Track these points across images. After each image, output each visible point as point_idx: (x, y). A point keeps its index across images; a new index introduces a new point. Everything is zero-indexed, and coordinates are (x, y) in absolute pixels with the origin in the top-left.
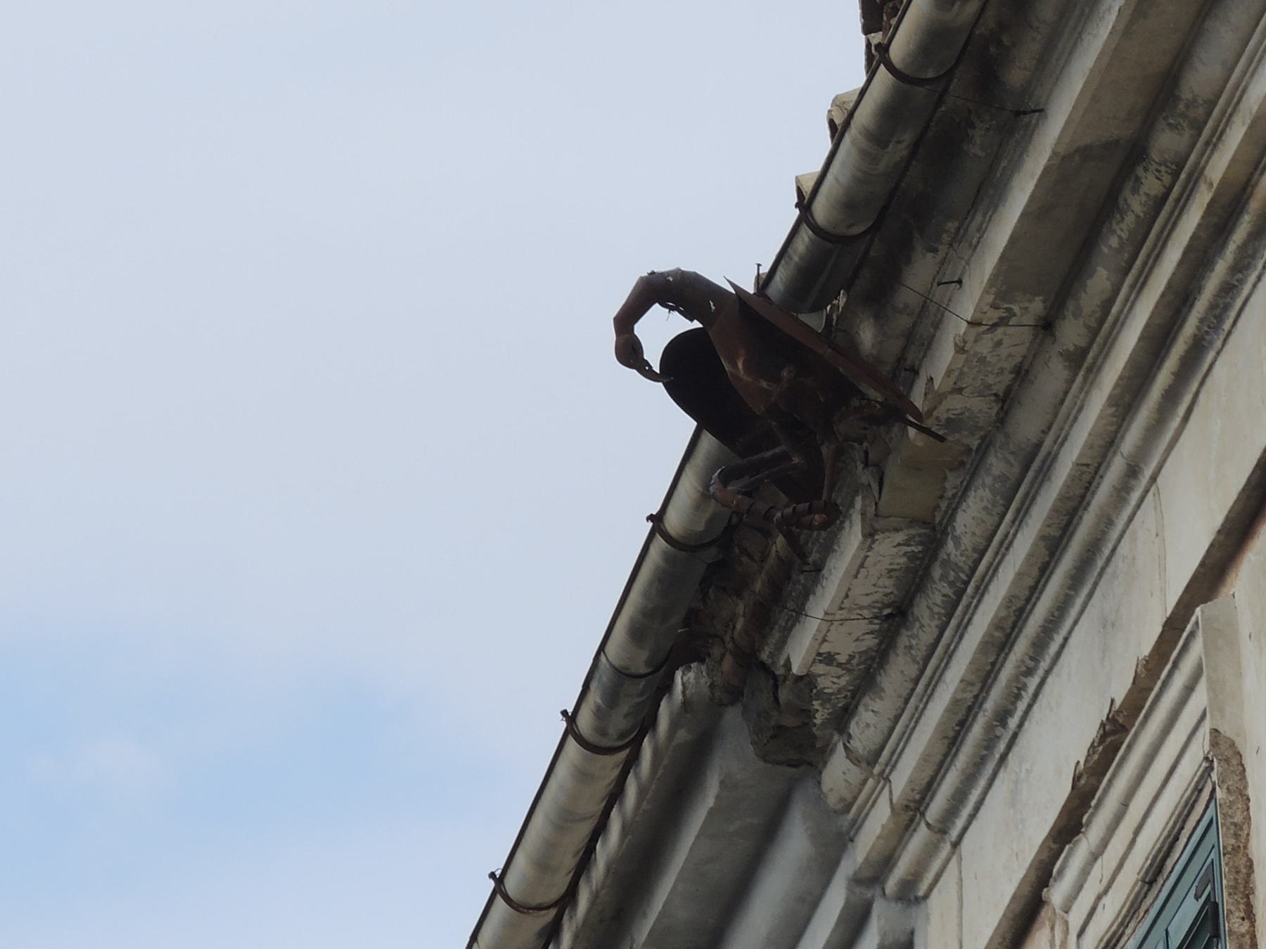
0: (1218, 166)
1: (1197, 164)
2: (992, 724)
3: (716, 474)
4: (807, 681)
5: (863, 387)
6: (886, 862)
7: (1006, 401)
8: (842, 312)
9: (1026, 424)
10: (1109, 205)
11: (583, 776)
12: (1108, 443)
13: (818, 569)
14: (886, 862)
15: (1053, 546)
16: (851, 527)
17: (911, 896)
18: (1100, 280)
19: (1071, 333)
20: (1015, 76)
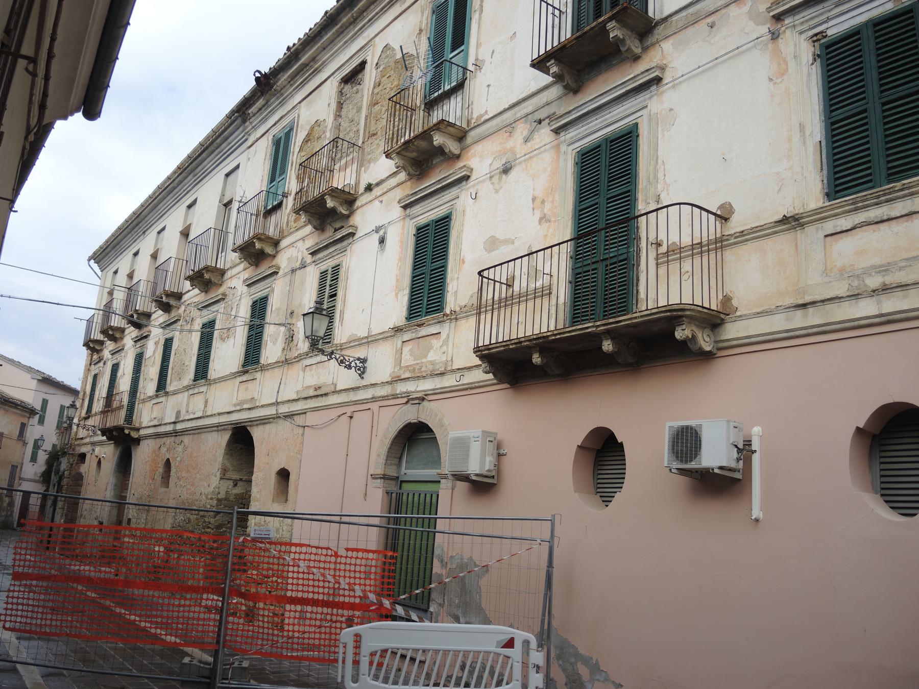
0: (316, 66)
1: (324, 62)
2: (225, 669)
3: (602, 18)
4: (249, 114)
5: (189, 650)
6: (248, 132)
7: (282, 89)
8: (165, 641)
9: (283, 91)
10: (302, 70)
11: (225, 120)
12: (291, 93)
13: (321, 37)
14: (248, 132)
15: (280, 103)
16: (109, 305)
17: (249, 135)
18: (298, 77)
19: (292, 82)
20: (300, 56)
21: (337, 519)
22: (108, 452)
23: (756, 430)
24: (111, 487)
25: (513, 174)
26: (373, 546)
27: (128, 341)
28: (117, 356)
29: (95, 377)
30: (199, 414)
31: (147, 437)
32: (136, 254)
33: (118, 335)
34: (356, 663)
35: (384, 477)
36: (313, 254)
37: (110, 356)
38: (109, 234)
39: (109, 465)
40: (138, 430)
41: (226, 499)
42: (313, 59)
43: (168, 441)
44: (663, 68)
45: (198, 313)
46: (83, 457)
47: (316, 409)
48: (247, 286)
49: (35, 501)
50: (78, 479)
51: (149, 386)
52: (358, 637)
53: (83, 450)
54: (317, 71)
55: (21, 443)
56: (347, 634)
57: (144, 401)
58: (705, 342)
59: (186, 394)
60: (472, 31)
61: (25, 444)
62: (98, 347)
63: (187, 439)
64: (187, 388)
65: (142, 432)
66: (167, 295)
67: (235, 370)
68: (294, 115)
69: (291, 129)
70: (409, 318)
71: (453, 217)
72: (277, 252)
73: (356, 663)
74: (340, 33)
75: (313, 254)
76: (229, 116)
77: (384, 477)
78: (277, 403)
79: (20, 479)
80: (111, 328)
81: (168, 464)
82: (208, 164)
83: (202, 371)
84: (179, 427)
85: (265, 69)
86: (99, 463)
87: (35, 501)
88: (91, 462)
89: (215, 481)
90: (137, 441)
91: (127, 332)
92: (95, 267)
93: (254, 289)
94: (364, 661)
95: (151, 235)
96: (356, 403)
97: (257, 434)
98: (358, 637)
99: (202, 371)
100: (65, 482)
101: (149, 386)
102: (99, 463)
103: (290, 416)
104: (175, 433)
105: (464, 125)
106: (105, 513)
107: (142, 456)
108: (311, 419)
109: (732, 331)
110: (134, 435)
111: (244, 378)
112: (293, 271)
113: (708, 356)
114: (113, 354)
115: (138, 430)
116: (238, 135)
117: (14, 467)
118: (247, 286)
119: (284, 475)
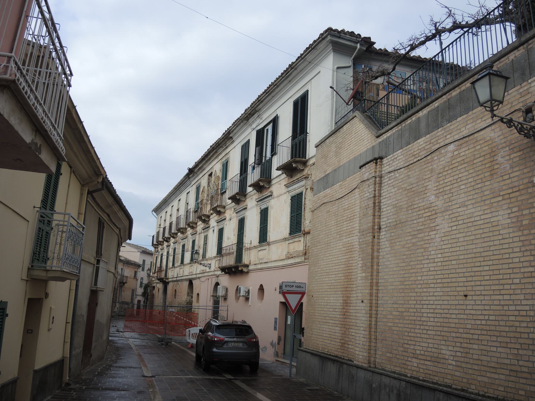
21: (205, 308)
22: (160, 286)
23: (251, 288)
24: (162, 299)
25: (232, 220)
26: (161, 305)
27: (213, 222)
28: (162, 251)
29: (157, 257)
30: (181, 275)
31: (171, 281)
32: (179, 200)
33: (194, 226)
34: (189, 336)
35: (213, 296)
36: (203, 230)
37: (216, 224)
38: (162, 199)
39: (161, 291)
40: (168, 279)
41: (189, 302)
42: (202, 166)
43: (176, 283)
44: (247, 205)
45: (181, 241)
46: (154, 287)
47: (203, 277)
48: (236, 213)
49: (142, 303)
50: (153, 295)
51: (170, 264)
52: (189, 331)
53: (154, 285)
54: (204, 170)
55: (135, 280)
56: (187, 330)
57: (250, 249)
58: (245, 270)
59: (179, 268)
60: (99, 278)
61: (137, 280)
62: (157, 247)
63: (180, 283)
64: (179, 266)
65: (170, 280)
66: (173, 234)
67: (189, 262)
68: (228, 156)
69: (227, 163)
70: (290, 234)
71: (269, 209)
72: (225, 210)
73: (189, 336)
74: (207, 162)
75: (203, 230)
76: (185, 176)
77: (213, 296)
78: (196, 274)
79: (136, 295)
80: (159, 241)
81: (176, 290)
82: (182, 188)
83: (182, 262)
84: (178, 279)
85: (191, 167)
86: (159, 290)
87: (142, 303)
88: (156, 289)
89: (186, 296)
90: (168, 283)
91: (198, 224)
92: (155, 214)
93: (238, 215)
94: (191, 335)
95: (170, 207)
96: (209, 276)
97: (194, 282)
98: (189, 331)
99: (182, 262)
100: (149, 297)
101: (170, 264)
102: (159, 290)
103: (199, 278)
104: (177, 281)
105: (225, 205)
106: (160, 309)
107: (170, 287)
108: (202, 279)
109: (251, 268)
110: (167, 281)
111: (190, 265)
112: (200, 234)
113: (248, 273)
114: (218, 222)
115: (168, 279)
116: (188, 182)
117: (133, 290)
118: (236, 213)
119: (198, 294)
